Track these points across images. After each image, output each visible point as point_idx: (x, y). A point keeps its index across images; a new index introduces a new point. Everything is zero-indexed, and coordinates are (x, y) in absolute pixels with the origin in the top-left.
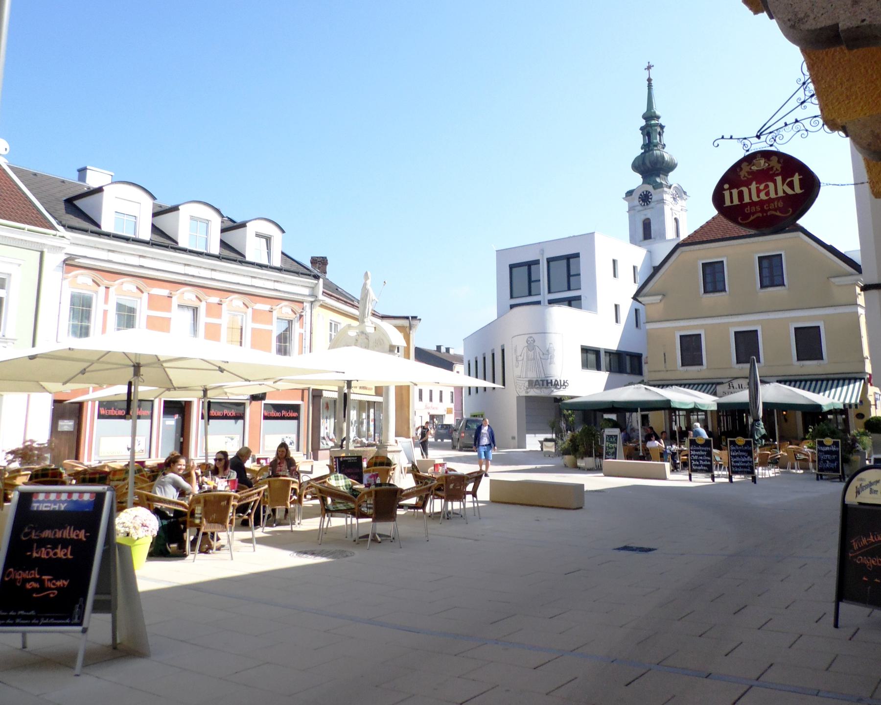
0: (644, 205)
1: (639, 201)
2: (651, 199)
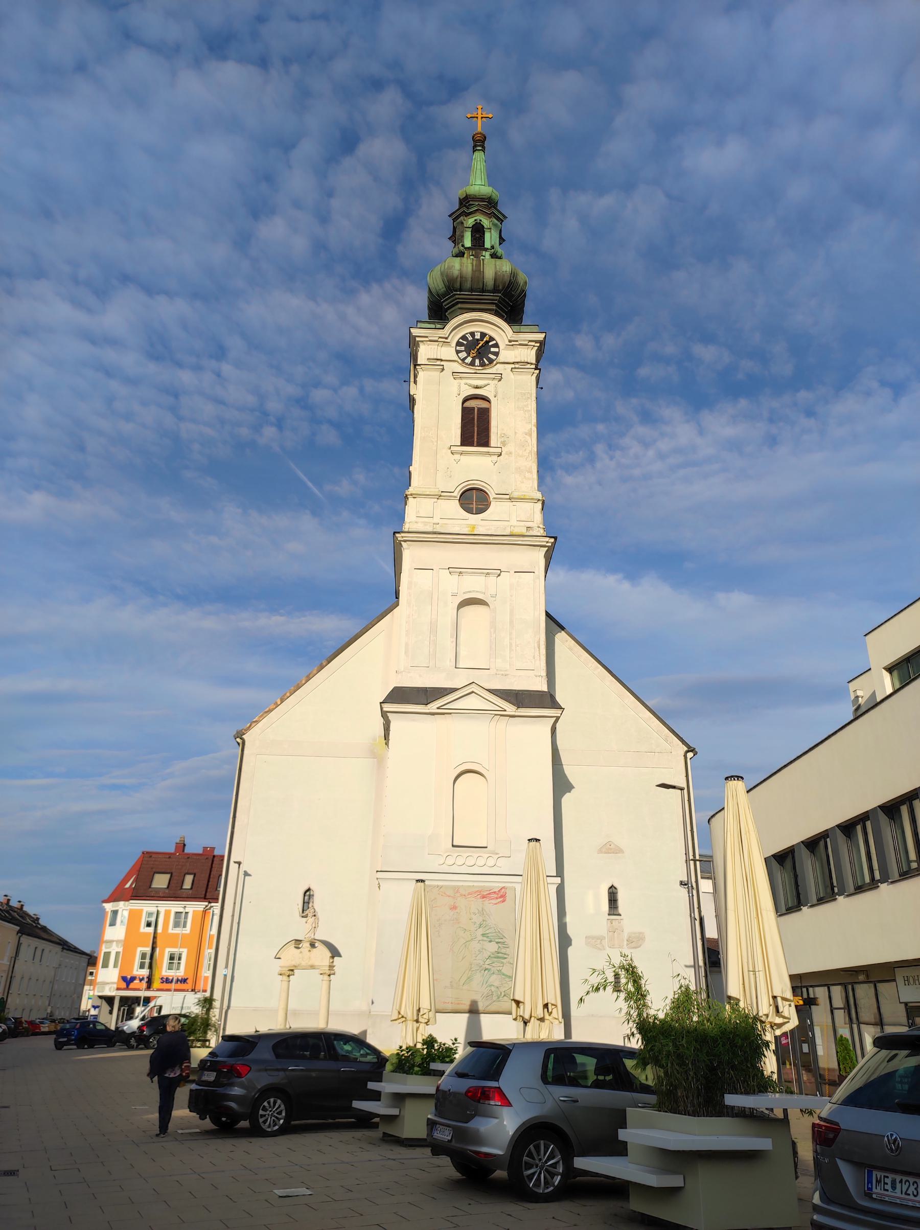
0: (472, 364)
1: (458, 352)
2: (497, 354)
